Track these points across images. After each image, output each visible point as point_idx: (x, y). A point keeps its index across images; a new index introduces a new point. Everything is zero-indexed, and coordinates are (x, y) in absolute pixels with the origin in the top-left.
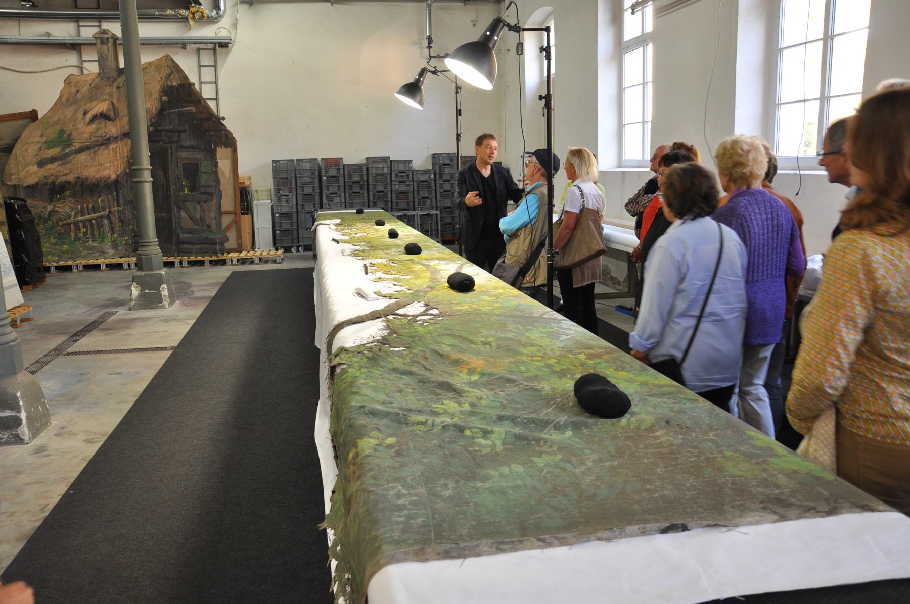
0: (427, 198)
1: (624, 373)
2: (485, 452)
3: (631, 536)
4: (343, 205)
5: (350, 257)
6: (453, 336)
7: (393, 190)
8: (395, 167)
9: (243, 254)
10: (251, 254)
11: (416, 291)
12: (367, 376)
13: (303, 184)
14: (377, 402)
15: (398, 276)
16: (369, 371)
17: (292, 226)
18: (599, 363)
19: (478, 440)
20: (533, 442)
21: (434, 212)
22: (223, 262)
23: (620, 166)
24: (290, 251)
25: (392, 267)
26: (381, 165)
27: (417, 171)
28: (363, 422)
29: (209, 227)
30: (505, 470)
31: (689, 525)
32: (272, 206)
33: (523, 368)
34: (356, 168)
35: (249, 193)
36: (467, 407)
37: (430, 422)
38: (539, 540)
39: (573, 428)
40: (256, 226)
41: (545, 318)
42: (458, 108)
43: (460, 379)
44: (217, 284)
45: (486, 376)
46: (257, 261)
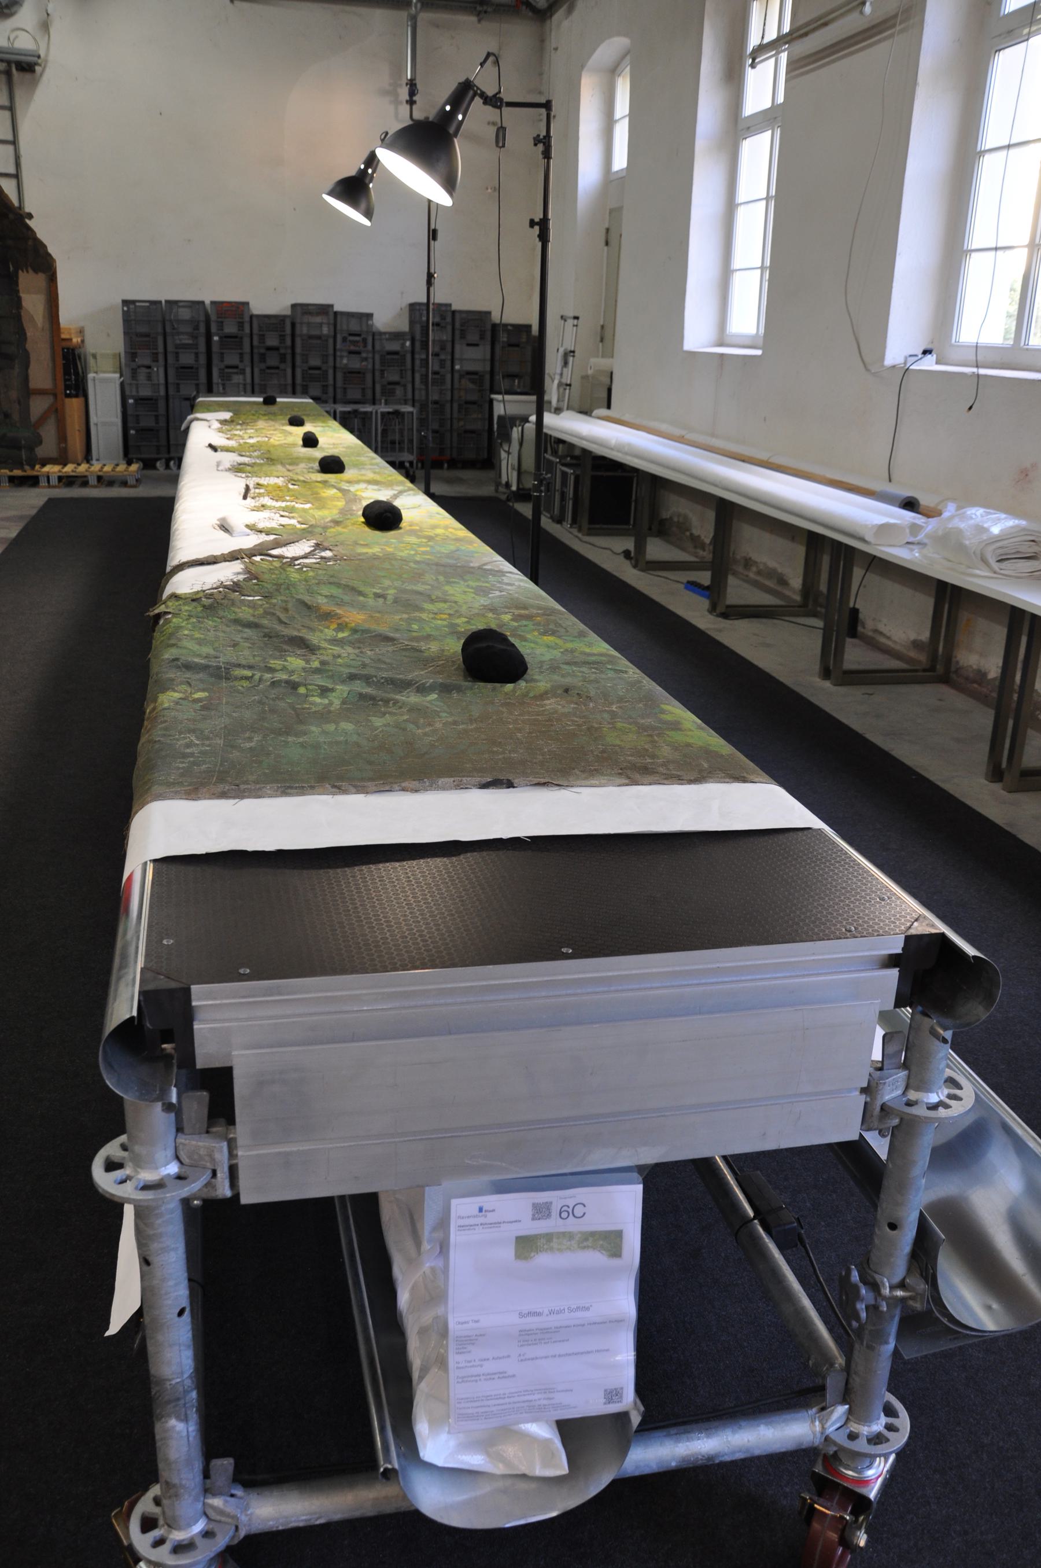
0: (397, 383)
1: (549, 639)
2: (314, 709)
3: (444, 788)
4: (249, 388)
5: (228, 474)
6: (338, 585)
7: (338, 365)
8: (343, 325)
9: (69, 469)
10: (83, 468)
11: (311, 526)
12: (194, 627)
13: (177, 347)
14: (199, 656)
15: (294, 503)
16: (199, 622)
17: (157, 423)
18: (525, 626)
19: (311, 699)
20: (380, 703)
21: (409, 409)
22: (33, 481)
23: (721, 344)
24: (154, 468)
25: (289, 490)
26: (318, 319)
27: (381, 334)
28: (173, 676)
29: (7, 415)
30: (332, 727)
31: (516, 782)
32: (122, 385)
33: (415, 627)
34: (274, 323)
35: (80, 358)
36: (316, 664)
37: (257, 677)
38: (334, 786)
39: (441, 691)
40: (93, 419)
41: (485, 569)
42: (432, 227)
43: (322, 635)
44: (21, 517)
45: (359, 634)
46: (93, 481)
